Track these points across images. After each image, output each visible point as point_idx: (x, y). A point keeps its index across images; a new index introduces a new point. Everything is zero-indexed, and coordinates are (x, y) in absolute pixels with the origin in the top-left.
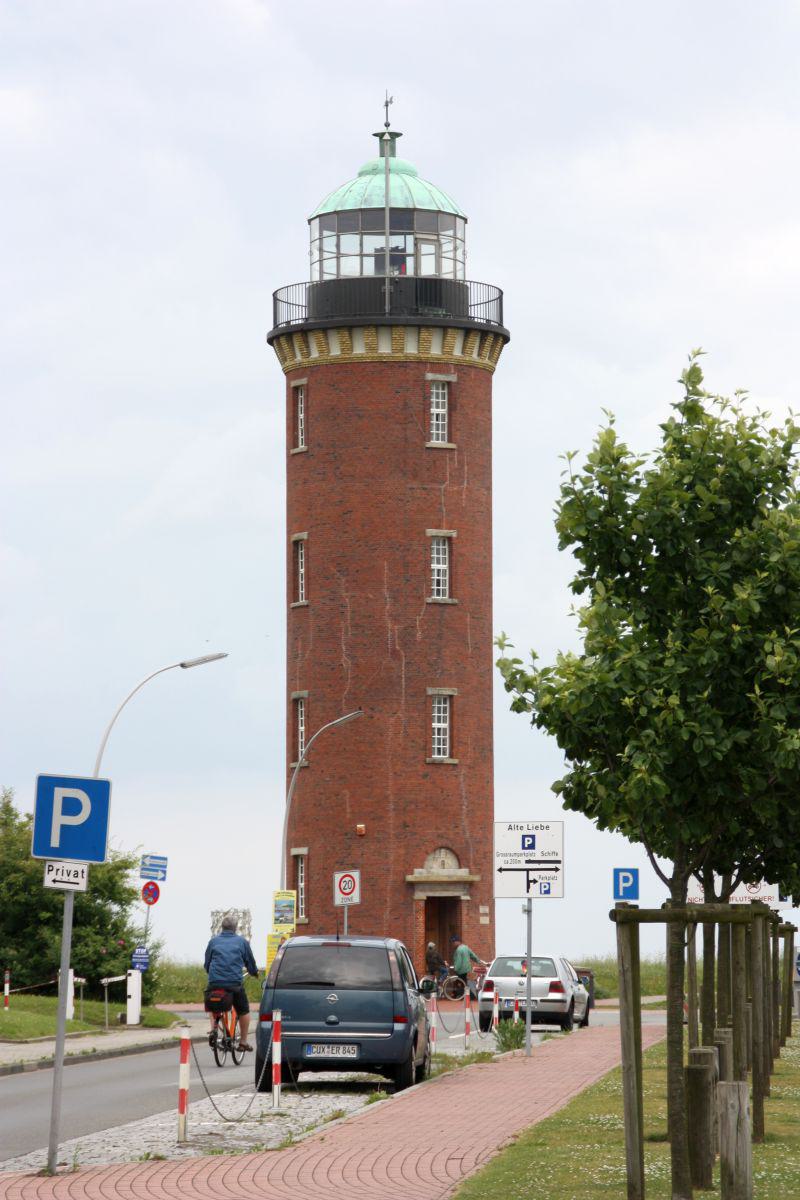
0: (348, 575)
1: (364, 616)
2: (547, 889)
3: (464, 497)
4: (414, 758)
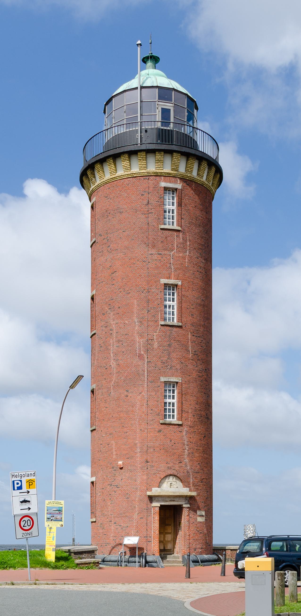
0: (114, 311)
2: (19, 485)
3: (187, 261)
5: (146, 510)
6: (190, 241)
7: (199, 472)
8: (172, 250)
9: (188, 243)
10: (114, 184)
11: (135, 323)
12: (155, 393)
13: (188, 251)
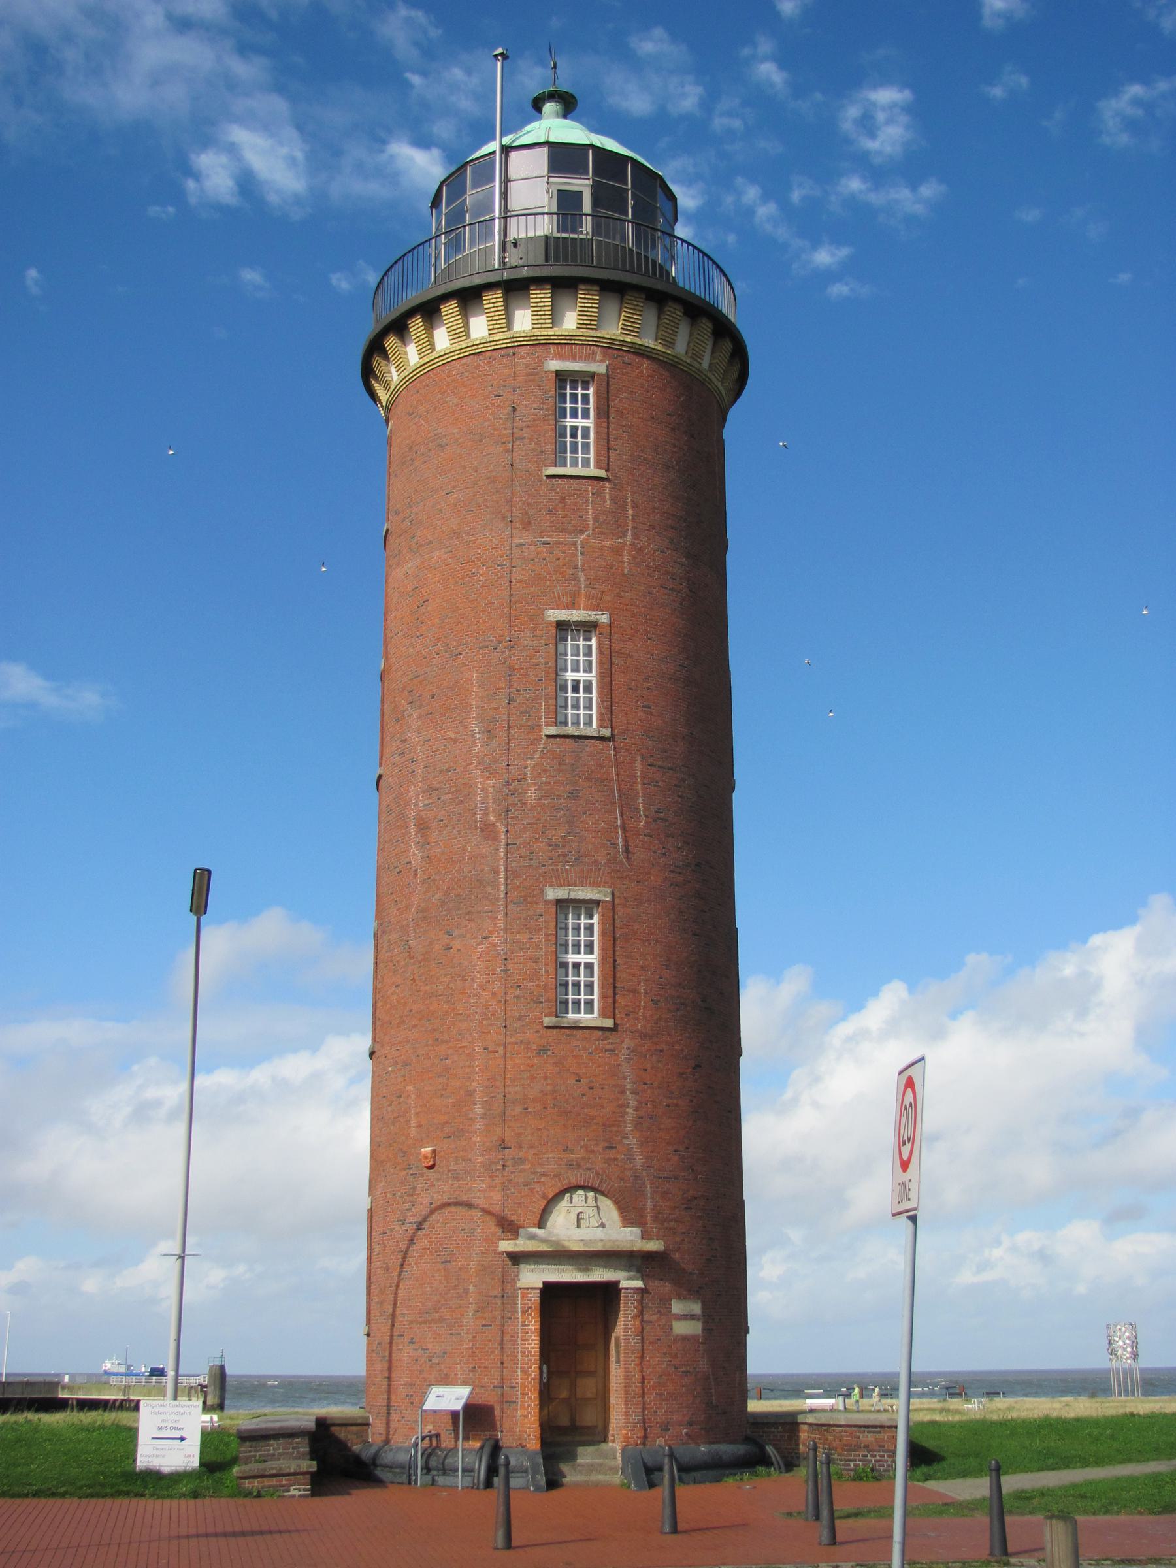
0: (420, 707)
1: (441, 771)
4: (520, 1018)
5: (498, 1301)
6: (635, 506)
7: (676, 1178)
8: (581, 532)
9: (630, 511)
10: (429, 377)
11: (473, 736)
12: (528, 936)
13: (629, 533)
